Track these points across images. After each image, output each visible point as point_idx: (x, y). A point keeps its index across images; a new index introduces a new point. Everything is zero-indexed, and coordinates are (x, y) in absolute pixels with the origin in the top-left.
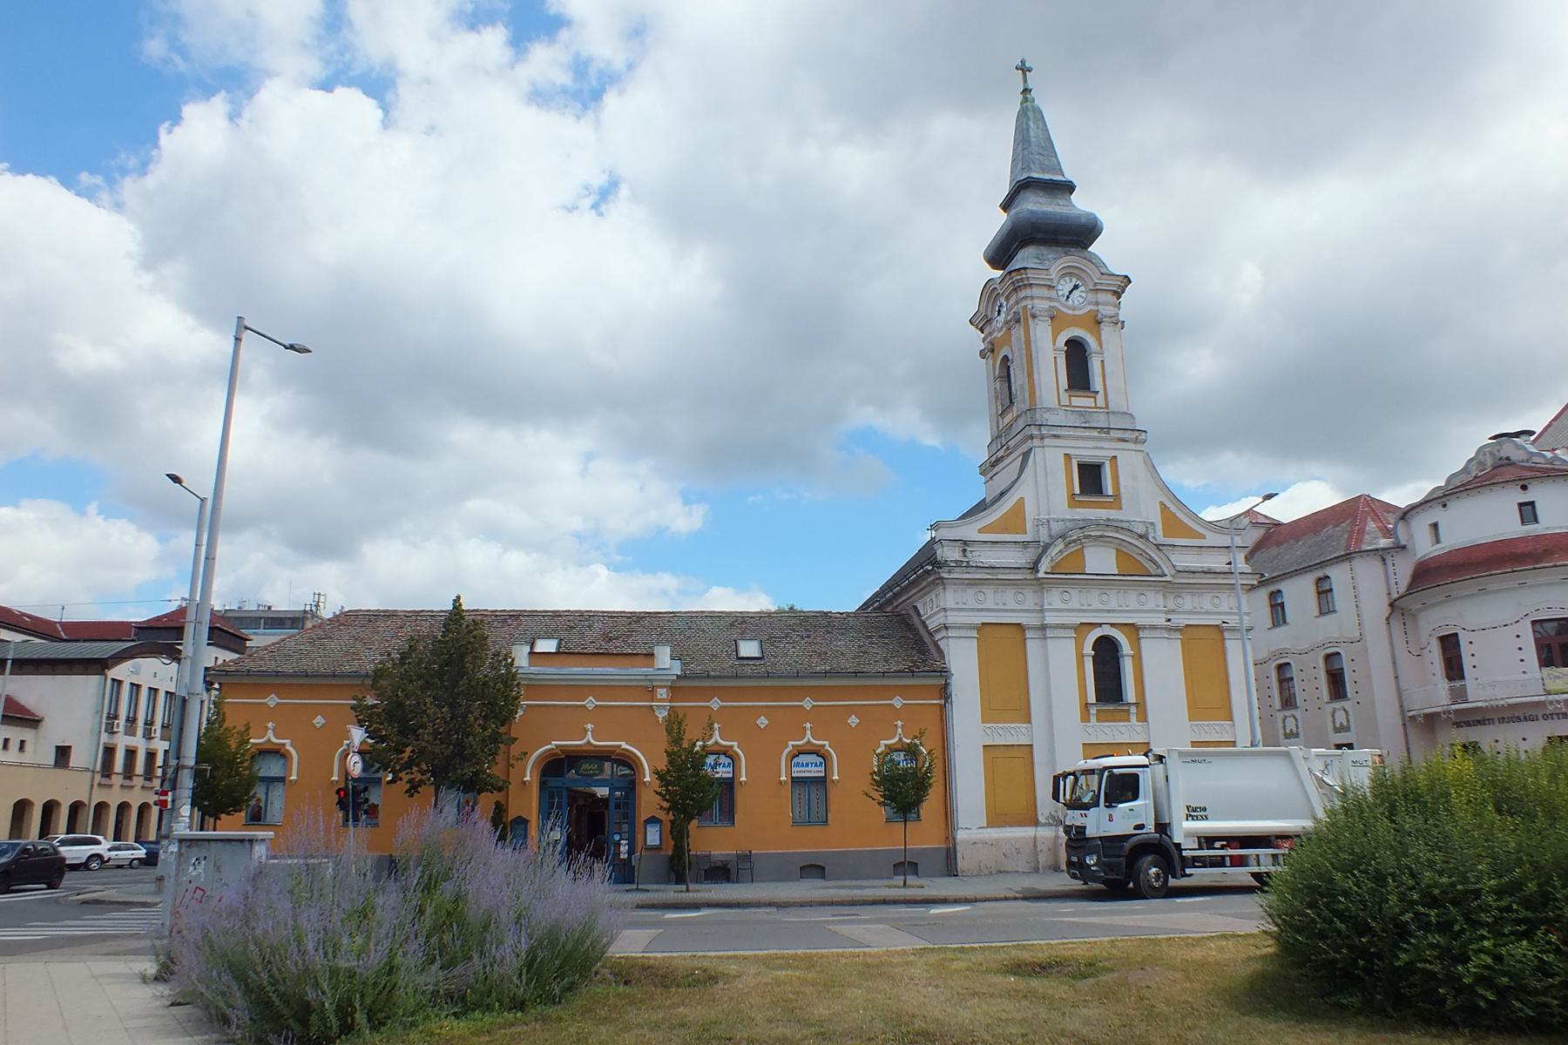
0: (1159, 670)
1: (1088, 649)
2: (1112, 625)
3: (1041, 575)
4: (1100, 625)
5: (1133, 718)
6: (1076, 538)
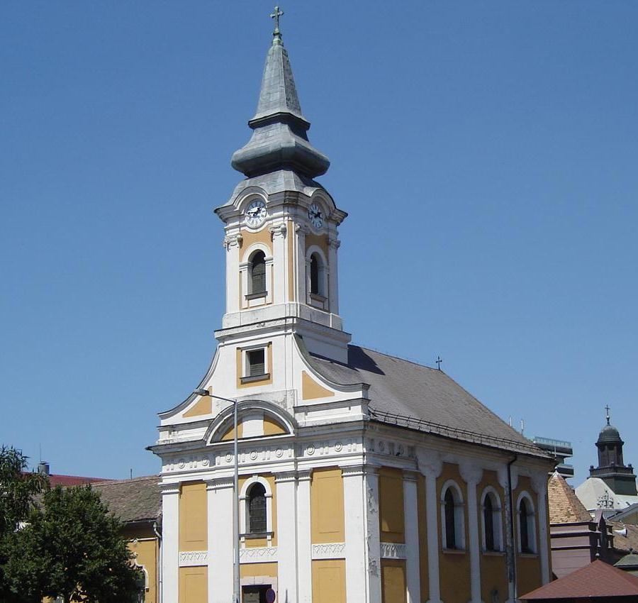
0: (290, 506)
1: (243, 494)
2: (260, 475)
3: (208, 444)
4: (250, 476)
5: (270, 543)
6: (244, 410)
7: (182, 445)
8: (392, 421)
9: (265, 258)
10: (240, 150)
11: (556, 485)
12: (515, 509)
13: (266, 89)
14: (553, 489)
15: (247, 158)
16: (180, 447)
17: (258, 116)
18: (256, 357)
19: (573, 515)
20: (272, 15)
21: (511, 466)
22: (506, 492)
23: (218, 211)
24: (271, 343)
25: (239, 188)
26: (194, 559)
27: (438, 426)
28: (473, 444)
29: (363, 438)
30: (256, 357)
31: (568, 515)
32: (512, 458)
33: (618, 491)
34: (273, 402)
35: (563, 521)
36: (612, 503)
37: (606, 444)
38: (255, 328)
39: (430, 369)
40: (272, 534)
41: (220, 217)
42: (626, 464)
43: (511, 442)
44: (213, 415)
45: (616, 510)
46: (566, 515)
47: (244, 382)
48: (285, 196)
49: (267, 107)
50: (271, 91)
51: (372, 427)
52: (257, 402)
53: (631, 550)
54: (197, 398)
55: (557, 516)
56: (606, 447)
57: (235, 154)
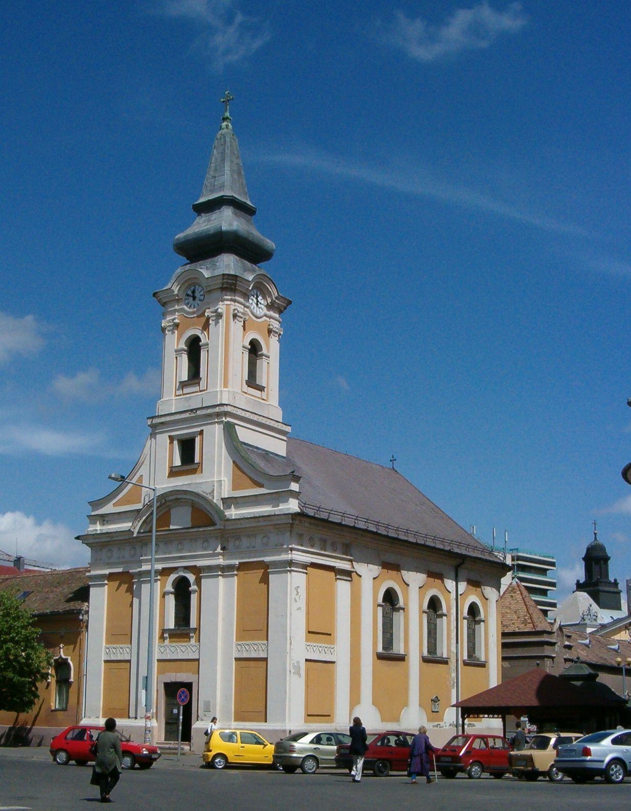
2: (186, 568)
6: (167, 503)
7: (109, 535)
8: (323, 516)
9: (200, 343)
10: (182, 233)
11: (515, 593)
12: (462, 613)
13: (212, 173)
14: (512, 596)
15: (189, 238)
16: (108, 537)
17: (202, 200)
18: (187, 447)
19: (529, 623)
20: (222, 100)
21: (460, 570)
22: (453, 595)
23: (157, 295)
24: (202, 431)
25: (179, 270)
26: (121, 653)
27: (377, 524)
28: (416, 544)
29: (291, 532)
30: (187, 447)
31: (525, 622)
32: (459, 561)
33: (602, 605)
34: (202, 493)
35: (519, 629)
36: (597, 617)
37: (602, 559)
38: (187, 415)
39: (383, 467)
40: (197, 630)
41: (159, 301)
42: (612, 580)
43: (475, 548)
44: (139, 506)
45: (600, 624)
46: (522, 623)
47: (174, 473)
48: (223, 279)
49: (212, 191)
50: (216, 175)
51: (300, 521)
52: (185, 492)
53: (578, 658)
54: (128, 486)
55: (513, 624)
56: (602, 561)
57: (176, 237)
